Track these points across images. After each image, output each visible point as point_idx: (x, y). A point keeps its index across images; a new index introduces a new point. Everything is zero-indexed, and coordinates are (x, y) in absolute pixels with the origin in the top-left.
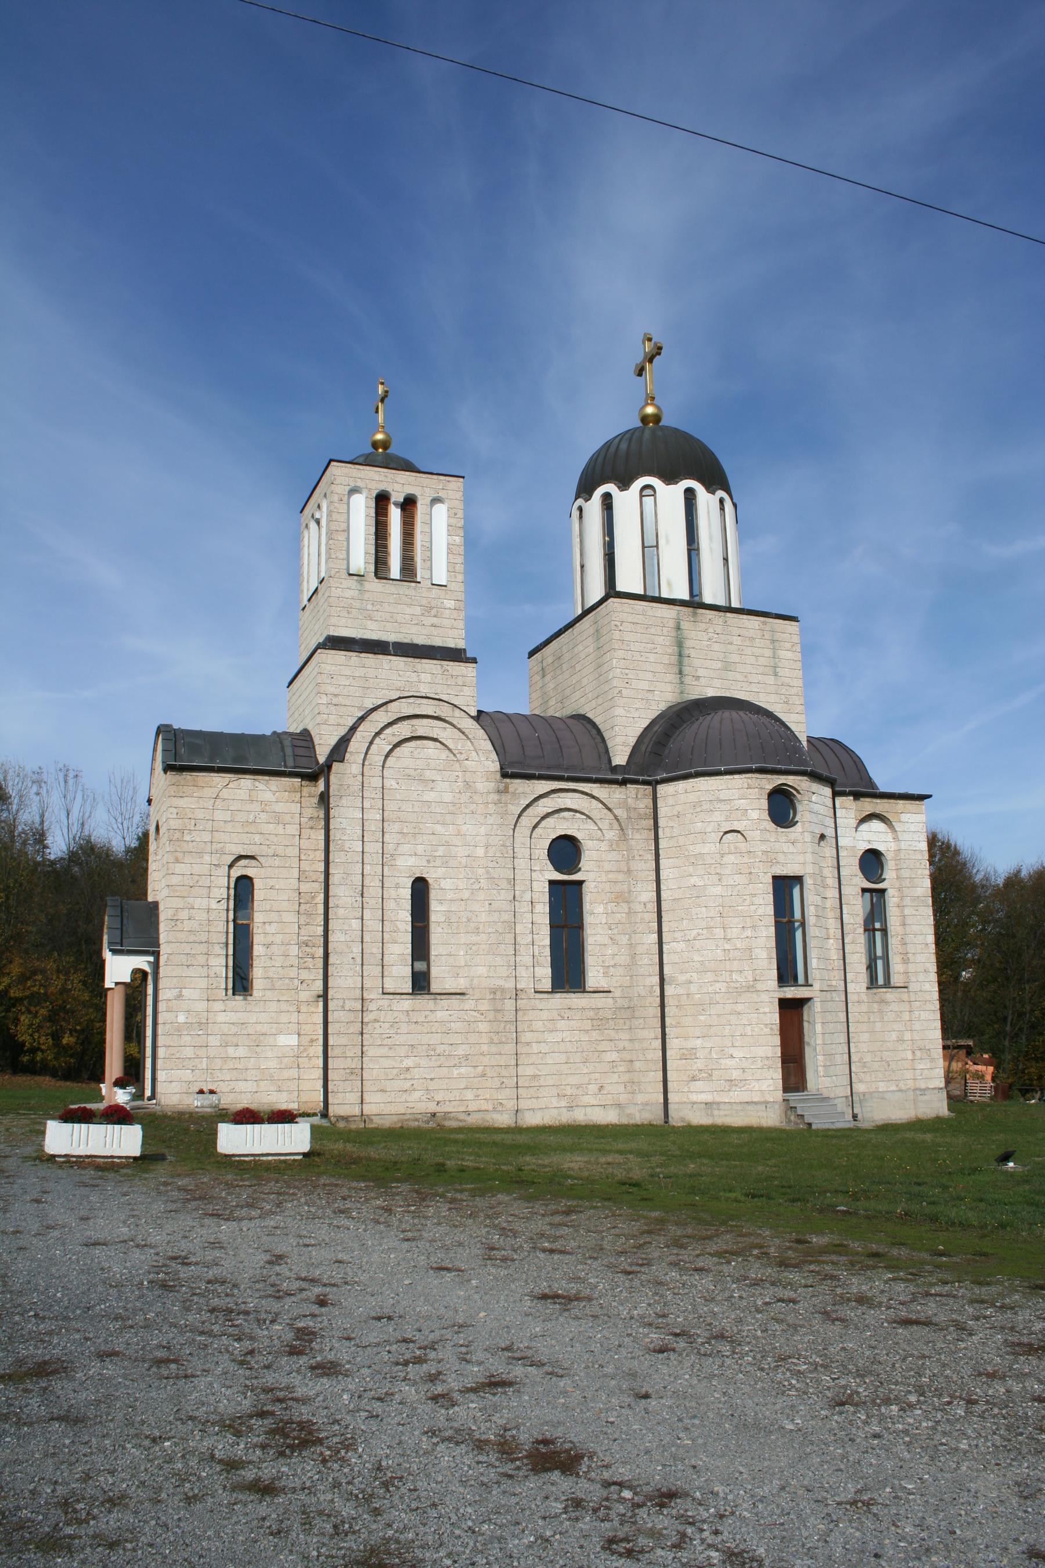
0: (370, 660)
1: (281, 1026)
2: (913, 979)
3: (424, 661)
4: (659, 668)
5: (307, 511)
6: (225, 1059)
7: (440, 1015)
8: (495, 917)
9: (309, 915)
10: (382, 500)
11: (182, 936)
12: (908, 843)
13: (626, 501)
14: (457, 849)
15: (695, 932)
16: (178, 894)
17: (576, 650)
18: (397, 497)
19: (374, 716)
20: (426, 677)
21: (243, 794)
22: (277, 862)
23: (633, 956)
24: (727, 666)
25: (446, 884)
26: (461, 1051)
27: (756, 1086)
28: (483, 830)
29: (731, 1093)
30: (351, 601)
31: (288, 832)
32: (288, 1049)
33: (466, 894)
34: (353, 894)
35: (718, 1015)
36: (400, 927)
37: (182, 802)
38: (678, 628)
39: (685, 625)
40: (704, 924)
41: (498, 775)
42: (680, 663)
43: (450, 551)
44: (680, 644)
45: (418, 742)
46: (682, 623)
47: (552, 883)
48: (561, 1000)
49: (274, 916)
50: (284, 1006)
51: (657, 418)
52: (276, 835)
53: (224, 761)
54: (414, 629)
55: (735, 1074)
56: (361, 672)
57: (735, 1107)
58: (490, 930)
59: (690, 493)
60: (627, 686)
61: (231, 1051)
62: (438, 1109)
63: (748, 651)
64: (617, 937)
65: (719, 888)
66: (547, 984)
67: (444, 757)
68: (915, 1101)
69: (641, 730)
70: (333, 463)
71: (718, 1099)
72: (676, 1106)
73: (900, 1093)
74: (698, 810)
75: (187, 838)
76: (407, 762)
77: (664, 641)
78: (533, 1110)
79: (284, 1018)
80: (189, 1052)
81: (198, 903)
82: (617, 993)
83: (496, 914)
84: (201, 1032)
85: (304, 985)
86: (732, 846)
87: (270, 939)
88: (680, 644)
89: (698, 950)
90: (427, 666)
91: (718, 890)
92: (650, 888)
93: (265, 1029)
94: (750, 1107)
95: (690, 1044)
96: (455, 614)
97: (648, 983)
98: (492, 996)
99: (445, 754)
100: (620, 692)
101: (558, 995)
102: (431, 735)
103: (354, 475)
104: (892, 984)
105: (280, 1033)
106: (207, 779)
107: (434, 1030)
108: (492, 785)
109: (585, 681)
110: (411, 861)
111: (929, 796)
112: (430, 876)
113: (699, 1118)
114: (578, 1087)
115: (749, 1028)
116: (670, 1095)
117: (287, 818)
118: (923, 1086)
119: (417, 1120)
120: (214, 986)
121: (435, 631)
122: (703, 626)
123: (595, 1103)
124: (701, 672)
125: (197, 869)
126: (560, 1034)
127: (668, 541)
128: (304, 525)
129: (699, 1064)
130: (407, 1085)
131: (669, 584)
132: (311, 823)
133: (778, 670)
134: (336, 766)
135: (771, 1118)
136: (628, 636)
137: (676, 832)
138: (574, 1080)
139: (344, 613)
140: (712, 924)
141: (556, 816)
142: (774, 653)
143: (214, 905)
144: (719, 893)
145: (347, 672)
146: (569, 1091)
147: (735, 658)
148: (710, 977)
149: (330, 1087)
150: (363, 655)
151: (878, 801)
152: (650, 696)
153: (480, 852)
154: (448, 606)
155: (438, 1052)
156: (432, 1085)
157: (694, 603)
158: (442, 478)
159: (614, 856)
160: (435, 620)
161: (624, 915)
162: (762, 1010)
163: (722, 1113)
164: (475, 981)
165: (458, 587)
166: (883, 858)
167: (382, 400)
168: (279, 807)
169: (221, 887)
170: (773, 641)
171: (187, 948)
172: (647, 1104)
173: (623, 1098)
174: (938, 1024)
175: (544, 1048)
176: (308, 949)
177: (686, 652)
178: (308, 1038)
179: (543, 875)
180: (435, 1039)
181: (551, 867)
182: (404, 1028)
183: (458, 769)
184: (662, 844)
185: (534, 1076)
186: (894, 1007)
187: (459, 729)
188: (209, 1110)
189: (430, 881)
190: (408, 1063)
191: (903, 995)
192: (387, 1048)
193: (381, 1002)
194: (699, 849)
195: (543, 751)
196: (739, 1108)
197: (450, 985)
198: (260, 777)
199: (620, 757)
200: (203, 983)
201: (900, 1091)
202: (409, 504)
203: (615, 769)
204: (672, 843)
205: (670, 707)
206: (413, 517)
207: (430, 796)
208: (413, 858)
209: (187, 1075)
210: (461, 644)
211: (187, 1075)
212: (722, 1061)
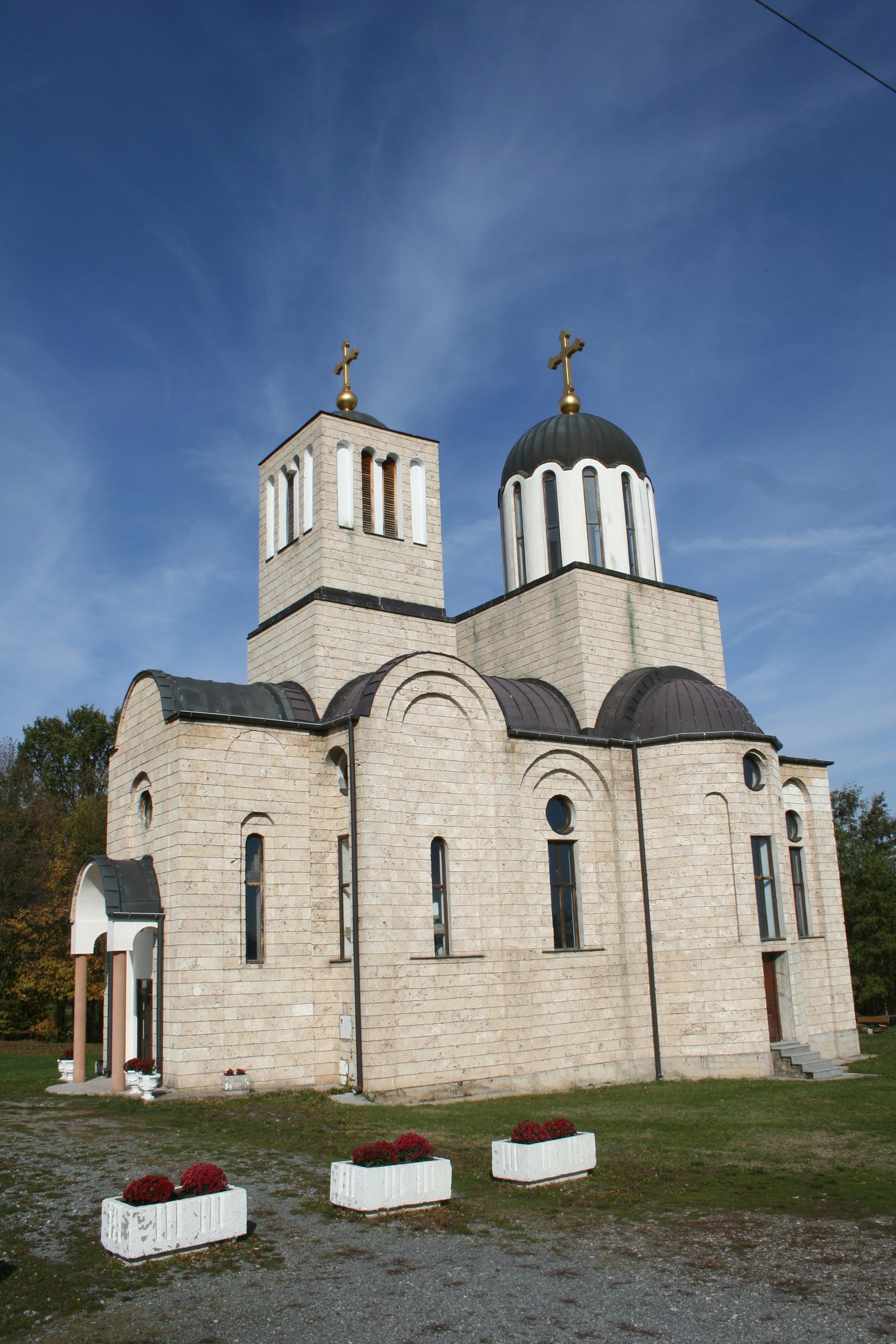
0: (362, 614)
1: (296, 995)
2: (829, 930)
3: (410, 618)
4: (616, 637)
5: (270, 463)
6: (242, 1034)
7: (463, 979)
8: (508, 877)
9: (320, 875)
10: (367, 455)
11: (196, 900)
12: (818, 805)
13: (570, 481)
14: (469, 808)
15: (682, 891)
16: (191, 854)
17: (524, 617)
18: (381, 454)
19: (396, 670)
20: (412, 635)
21: (253, 747)
22: (288, 820)
23: (622, 915)
24: (668, 639)
25: (461, 844)
26: (482, 1015)
27: (746, 1037)
28: (492, 789)
29: (725, 1046)
30: (343, 554)
31: (298, 788)
32: (304, 1019)
33: (481, 854)
34: (382, 855)
35: (710, 970)
36: (422, 888)
37: (194, 754)
38: (629, 601)
39: (634, 598)
40: (692, 883)
41: (506, 734)
42: (632, 634)
43: (429, 513)
44: (631, 615)
45: (432, 699)
46: (632, 596)
47: (551, 842)
48: (566, 959)
49: (287, 878)
50: (299, 974)
51: (576, 408)
52: (287, 791)
53: (223, 711)
54: (399, 587)
55: (728, 1027)
56: (353, 626)
57: (729, 1059)
58: (505, 890)
59: (625, 476)
60: (592, 652)
61: (248, 1025)
62: (464, 1077)
63: (682, 625)
64: (607, 896)
65: (705, 848)
66: (550, 944)
67: (455, 715)
68: (836, 1043)
69: (605, 695)
70: (323, 415)
71: (713, 1052)
72: (669, 1060)
73: (824, 1036)
74: (681, 772)
75: (200, 792)
76: (423, 719)
77: (619, 612)
78: (546, 1071)
79: (299, 986)
80: (205, 1028)
81: (212, 863)
82: (609, 950)
83: (510, 874)
84: (217, 1005)
85: (317, 950)
86: (713, 808)
87: (283, 902)
88: (631, 615)
89: (686, 908)
90: (414, 624)
91: (704, 850)
92: (634, 848)
93: (280, 999)
94: (743, 1059)
95: (680, 999)
96: (435, 574)
97: (636, 940)
98: (508, 958)
99: (456, 712)
100: (587, 658)
101: (562, 955)
102: (444, 693)
103: (342, 429)
104: (810, 934)
105: (296, 1002)
106: (218, 730)
107: (457, 995)
108: (500, 745)
109: (538, 647)
110: (430, 820)
111: (831, 763)
112: (447, 836)
113: (695, 1073)
114: (582, 1045)
115: (738, 982)
116: (661, 1050)
117: (297, 773)
118: (841, 1028)
119: (446, 1090)
120: (229, 954)
121: (418, 590)
122: (647, 600)
123: (596, 1061)
124: (648, 643)
125: (210, 827)
126: (564, 993)
127: (610, 520)
128: (267, 476)
129: (692, 1018)
130: (435, 1054)
131: (613, 559)
132: (319, 779)
133: (705, 644)
134: (362, 719)
135: (760, 1068)
136: (592, 606)
137: (659, 793)
138: (577, 1039)
139: (336, 566)
140: (699, 882)
141: (551, 776)
142: (701, 628)
143: (228, 866)
144: (704, 852)
145: (342, 624)
146: (575, 1050)
147: (672, 631)
148: (700, 933)
149: (365, 1062)
150: (356, 609)
151: (796, 766)
152: (610, 663)
153: (491, 811)
154: (429, 565)
155: (462, 1018)
156: (458, 1053)
157: (634, 577)
158: (419, 440)
159: (600, 816)
160: (417, 579)
161: (612, 874)
162: (749, 964)
163: (717, 1065)
164: (492, 942)
165: (436, 547)
166: (797, 819)
167: (348, 362)
168: (289, 762)
169: (236, 848)
170: (700, 618)
171: (201, 913)
172: (641, 1060)
173: (620, 1055)
174: (848, 970)
175: (553, 1008)
176: (320, 912)
177: (636, 624)
178: (322, 1007)
179: (543, 835)
180: (458, 1004)
181: (549, 827)
182: (431, 995)
183: (468, 727)
184: (645, 805)
185: (546, 1038)
186: (816, 956)
187: (470, 688)
188: (240, 1093)
189: (447, 841)
190: (436, 1030)
191: (820, 943)
192: (416, 1016)
193: (409, 968)
194: (683, 810)
195: (534, 712)
196: (733, 1059)
197: (469, 948)
198: (270, 730)
199: (589, 721)
200: (218, 951)
201: (824, 1033)
202: (389, 464)
203: (586, 731)
204: (656, 804)
205: (626, 675)
206: (393, 477)
207: (444, 754)
208: (432, 818)
209: (204, 1053)
210: (441, 604)
211: (204, 1053)
212: (715, 1015)
